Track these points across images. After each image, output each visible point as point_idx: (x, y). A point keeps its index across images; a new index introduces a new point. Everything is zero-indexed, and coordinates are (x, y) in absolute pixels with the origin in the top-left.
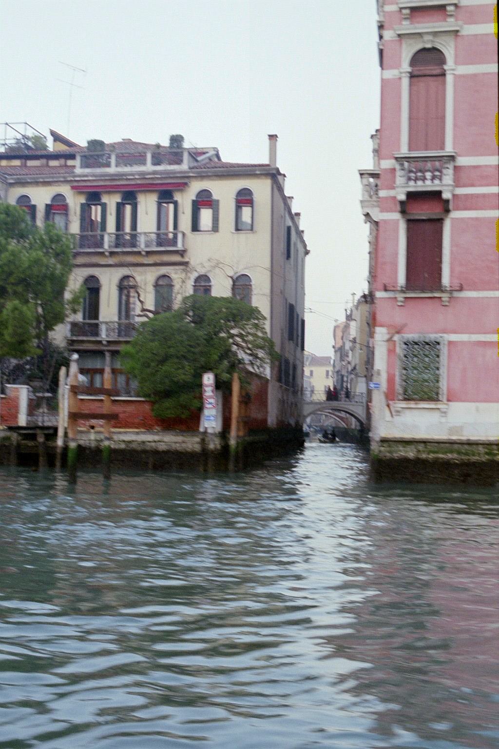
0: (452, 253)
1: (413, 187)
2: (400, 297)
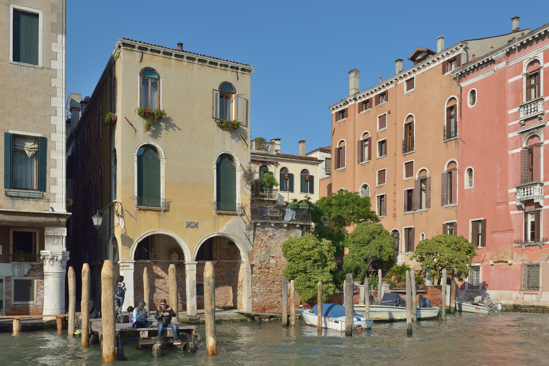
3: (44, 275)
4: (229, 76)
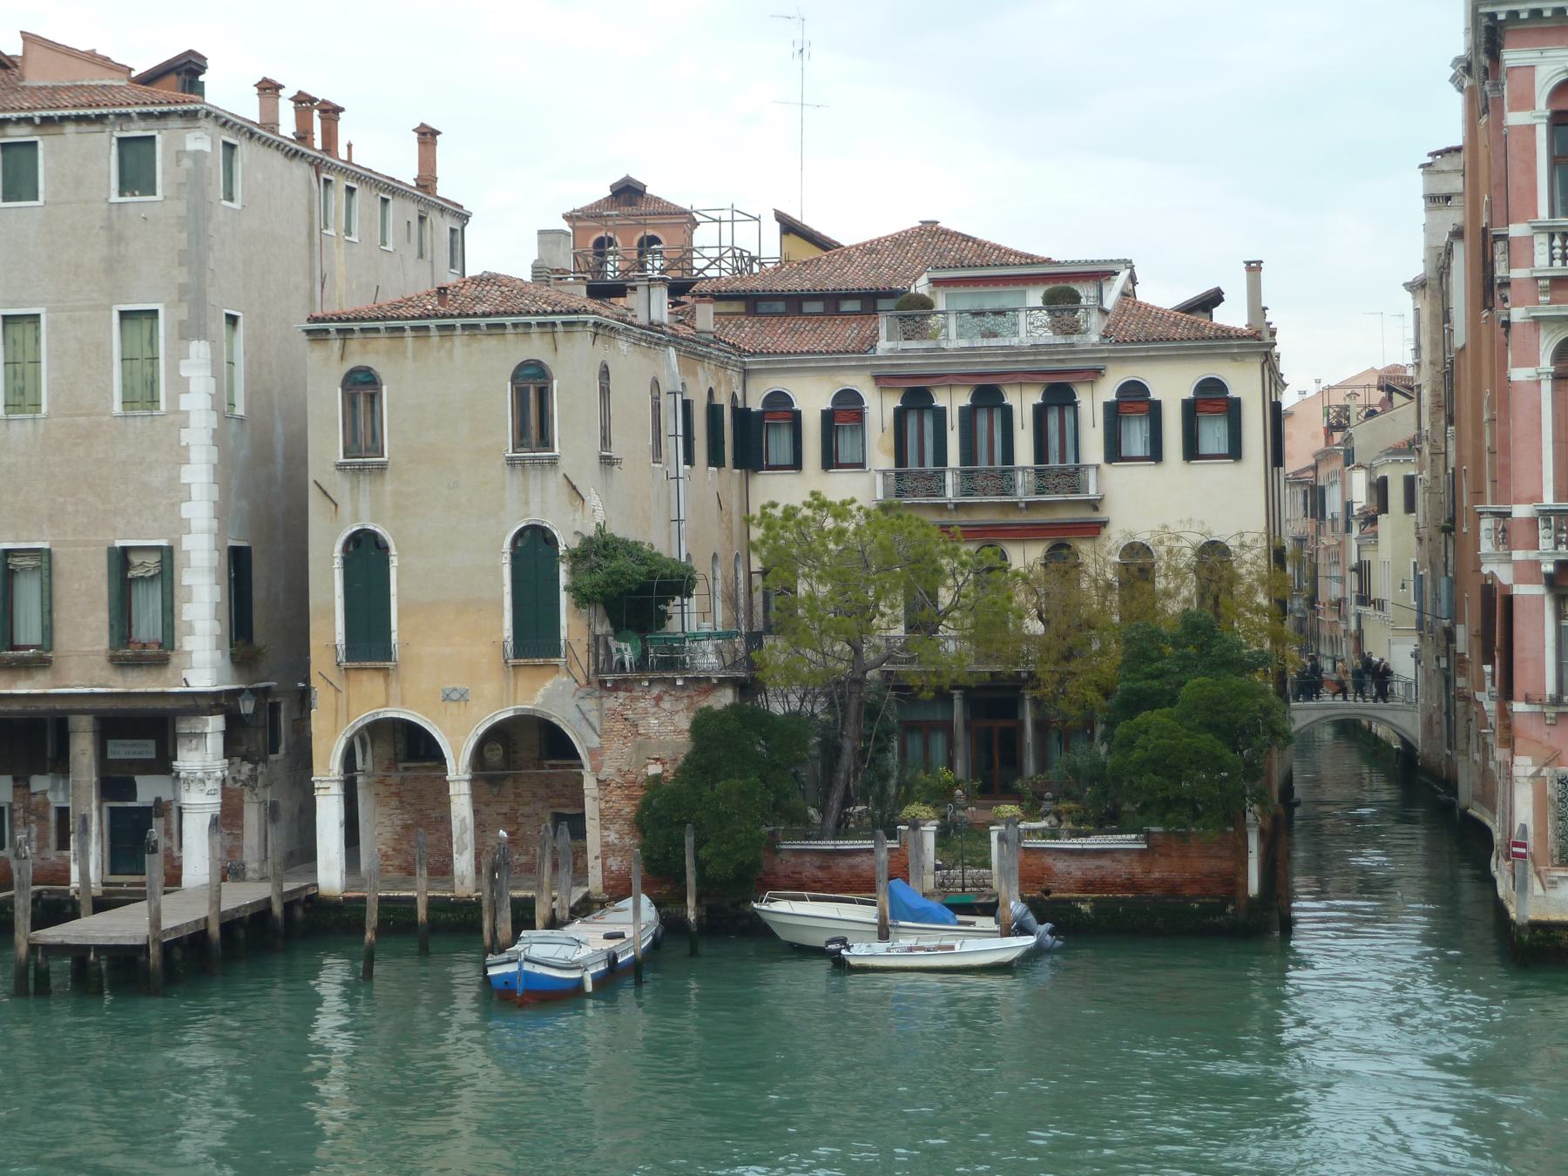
2: (1551, 712)
3: (313, 789)
4: (535, 348)
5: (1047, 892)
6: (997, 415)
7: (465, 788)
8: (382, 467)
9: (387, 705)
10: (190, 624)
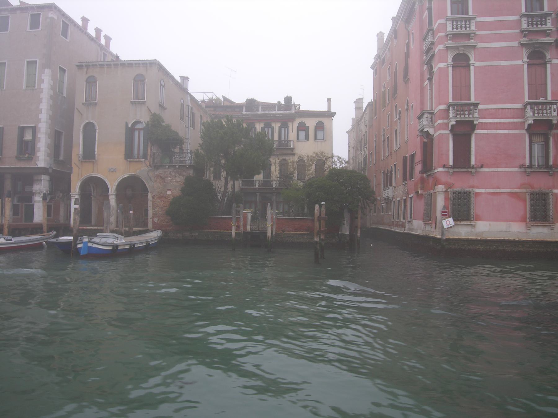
0: (475, 150)
1: (459, 118)
2: (451, 171)
5: (283, 231)
6: (270, 130)
7: (114, 197)
8: (96, 104)
9: (93, 172)
10: (39, 148)
